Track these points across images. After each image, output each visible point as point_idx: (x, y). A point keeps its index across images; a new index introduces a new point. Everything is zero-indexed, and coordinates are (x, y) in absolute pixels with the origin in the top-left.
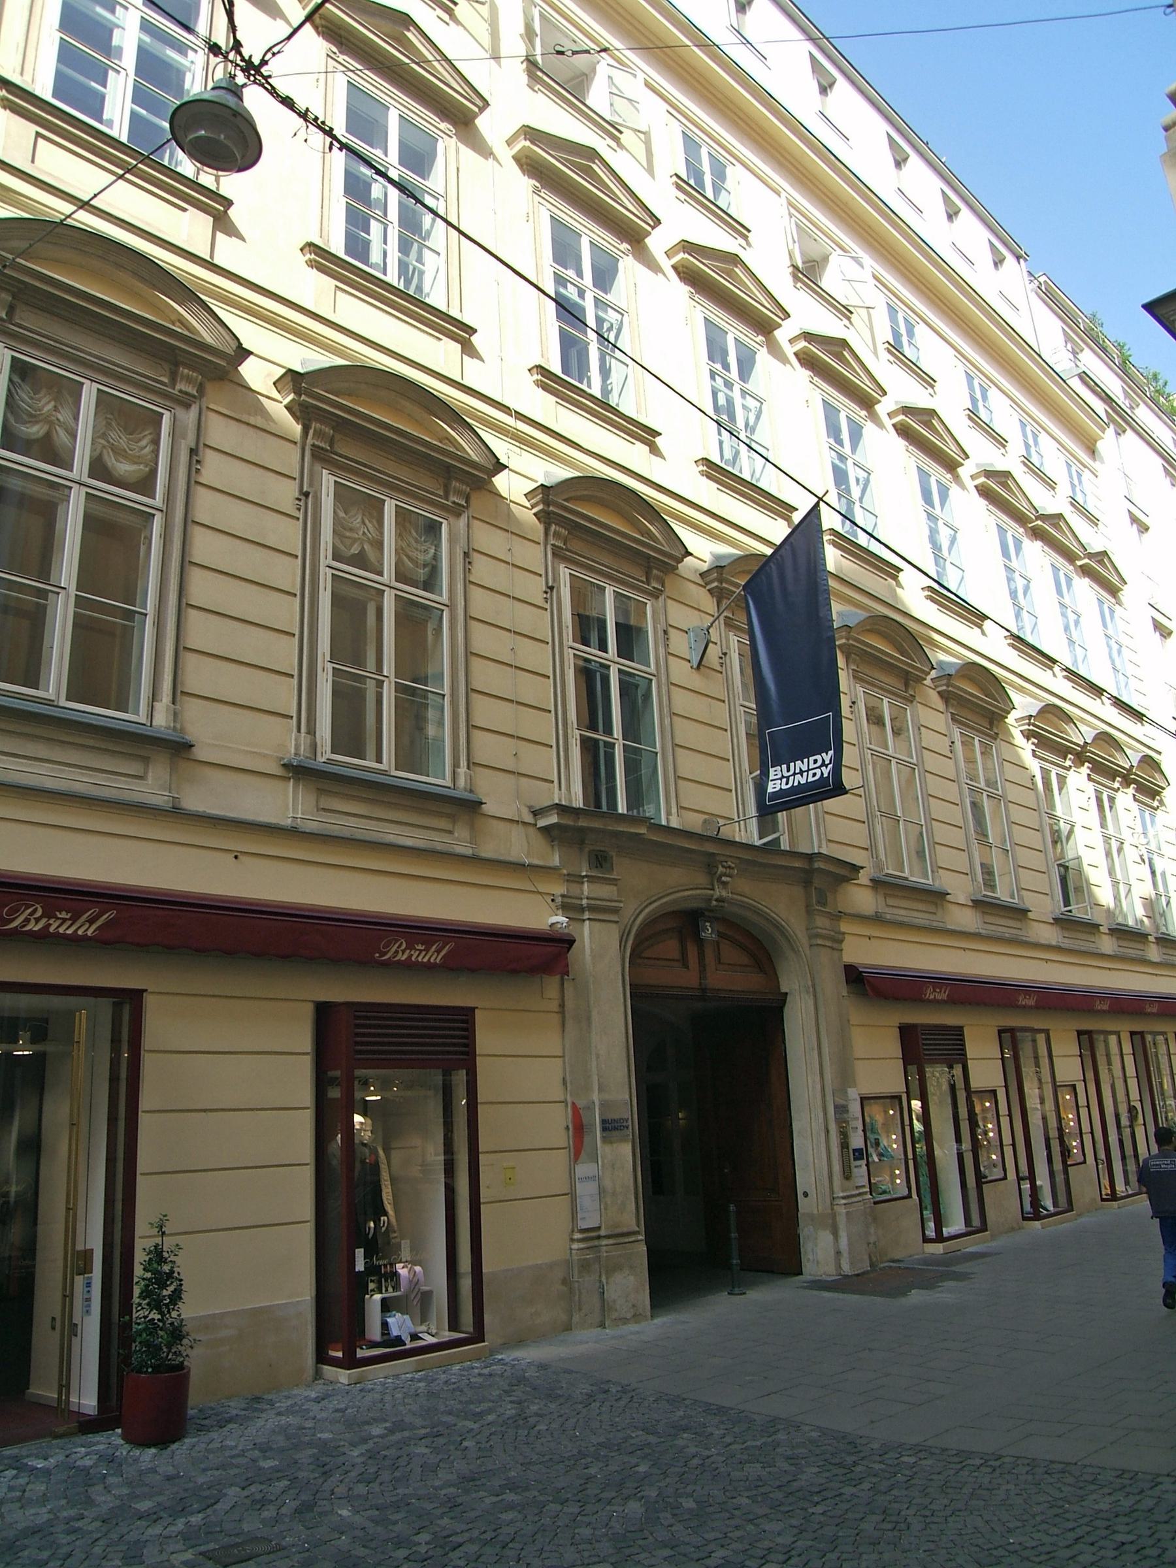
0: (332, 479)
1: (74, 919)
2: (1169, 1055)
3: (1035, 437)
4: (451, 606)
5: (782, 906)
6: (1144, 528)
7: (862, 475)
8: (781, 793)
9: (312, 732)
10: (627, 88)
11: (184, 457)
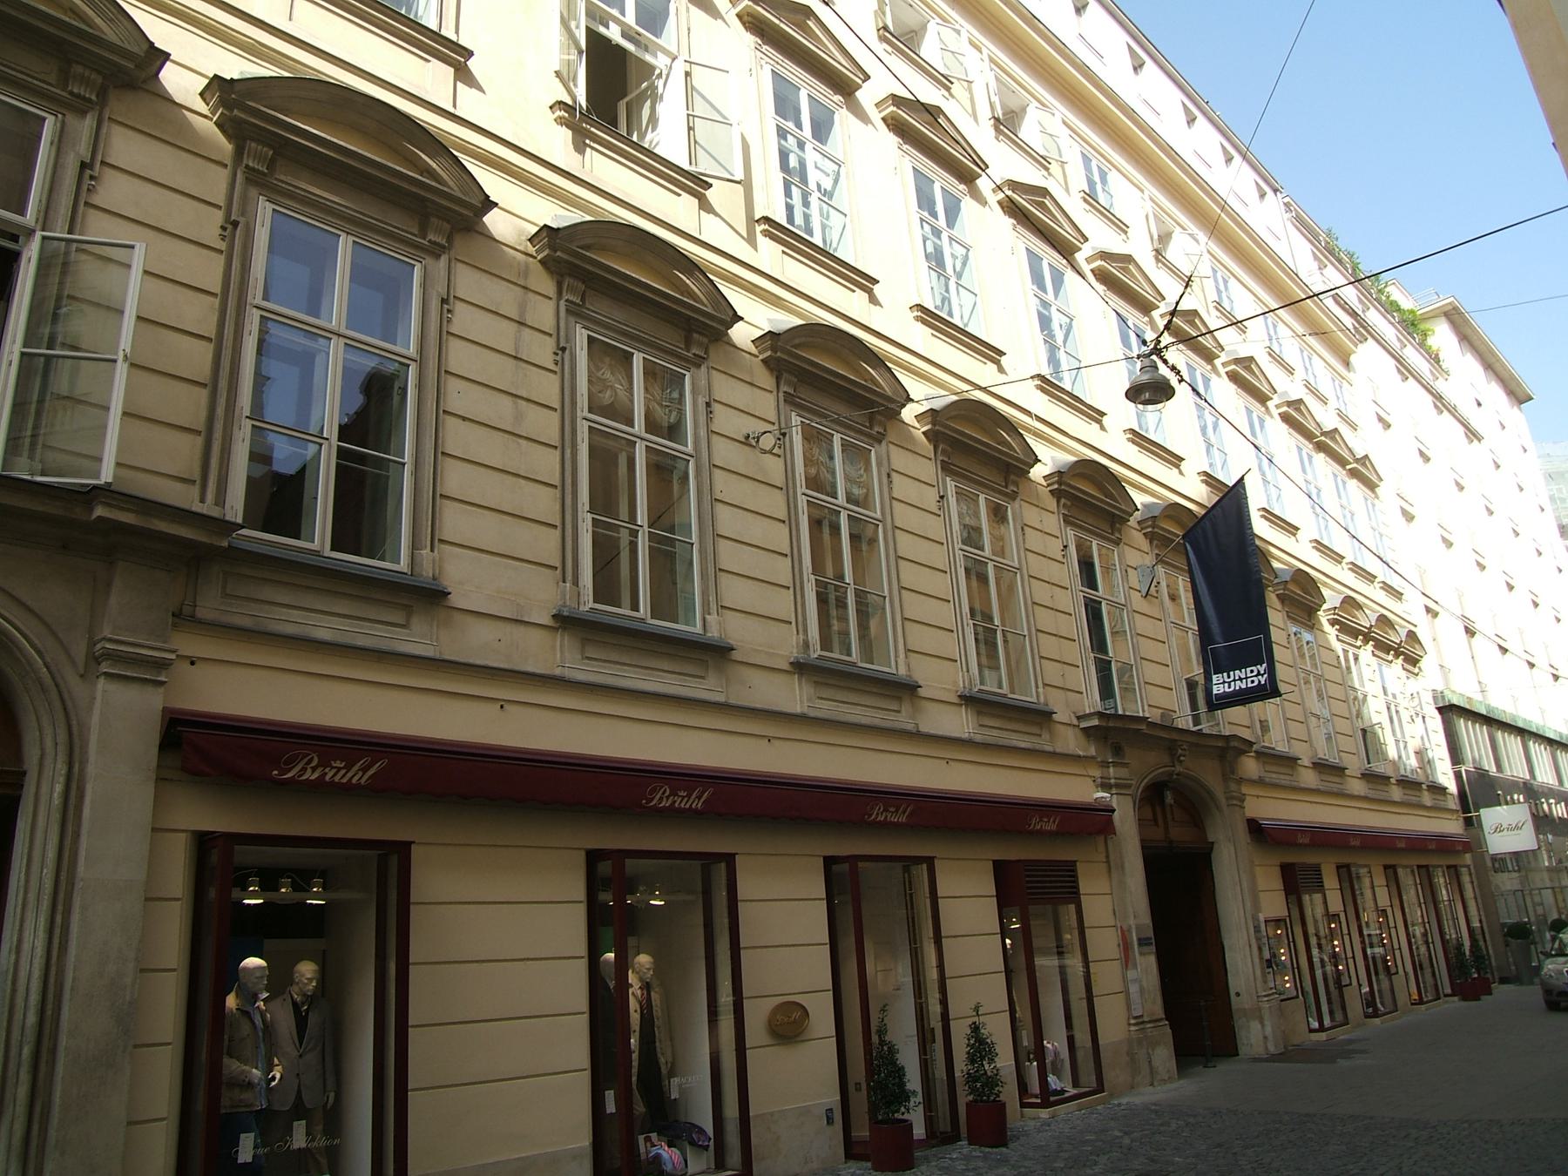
0: (585, 333)
1: (348, 768)
2: (1373, 888)
3: (1225, 282)
4: (697, 456)
5: (1208, 774)
6: (1387, 426)
7: (960, 251)
8: (1225, 695)
9: (576, 582)
10: (952, 43)
11: (434, 304)
